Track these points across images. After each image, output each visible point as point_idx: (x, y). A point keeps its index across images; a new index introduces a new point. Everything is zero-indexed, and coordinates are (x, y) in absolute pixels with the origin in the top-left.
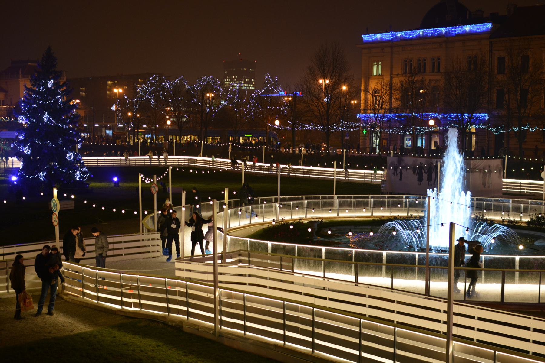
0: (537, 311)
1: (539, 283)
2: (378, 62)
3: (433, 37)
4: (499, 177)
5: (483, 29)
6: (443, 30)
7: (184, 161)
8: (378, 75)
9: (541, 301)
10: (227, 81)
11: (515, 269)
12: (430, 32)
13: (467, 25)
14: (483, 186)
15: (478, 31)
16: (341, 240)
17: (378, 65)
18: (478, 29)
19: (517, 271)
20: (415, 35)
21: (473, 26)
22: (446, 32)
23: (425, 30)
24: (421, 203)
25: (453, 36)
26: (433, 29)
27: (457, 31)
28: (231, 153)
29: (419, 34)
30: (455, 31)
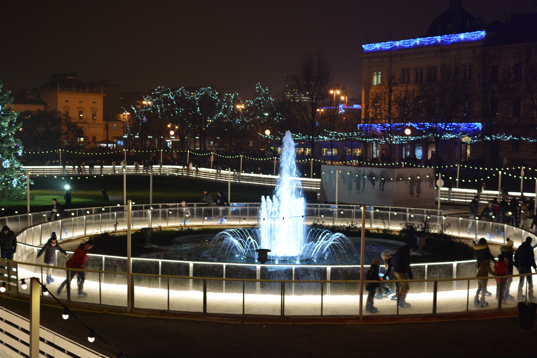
0: (237, 323)
1: (242, 292)
2: (377, 72)
3: (429, 46)
4: (430, 186)
5: (477, 37)
6: (439, 38)
7: (169, 170)
8: (378, 85)
9: (245, 313)
10: (288, 94)
11: (189, 276)
12: (426, 40)
13: (461, 33)
14: (410, 195)
15: (473, 39)
16: (181, 247)
17: (378, 75)
18: (472, 37)
19: (191, 278)
20: (412, 44)
21: (467, 34)
22: (442, 41)
23: (422, 39)
24: (248, 210)
25: (449, 45)
26: (429, 38)
27: (452, 39)
28: (213, 162)
29: (416, 43)
30: (450, 39)
